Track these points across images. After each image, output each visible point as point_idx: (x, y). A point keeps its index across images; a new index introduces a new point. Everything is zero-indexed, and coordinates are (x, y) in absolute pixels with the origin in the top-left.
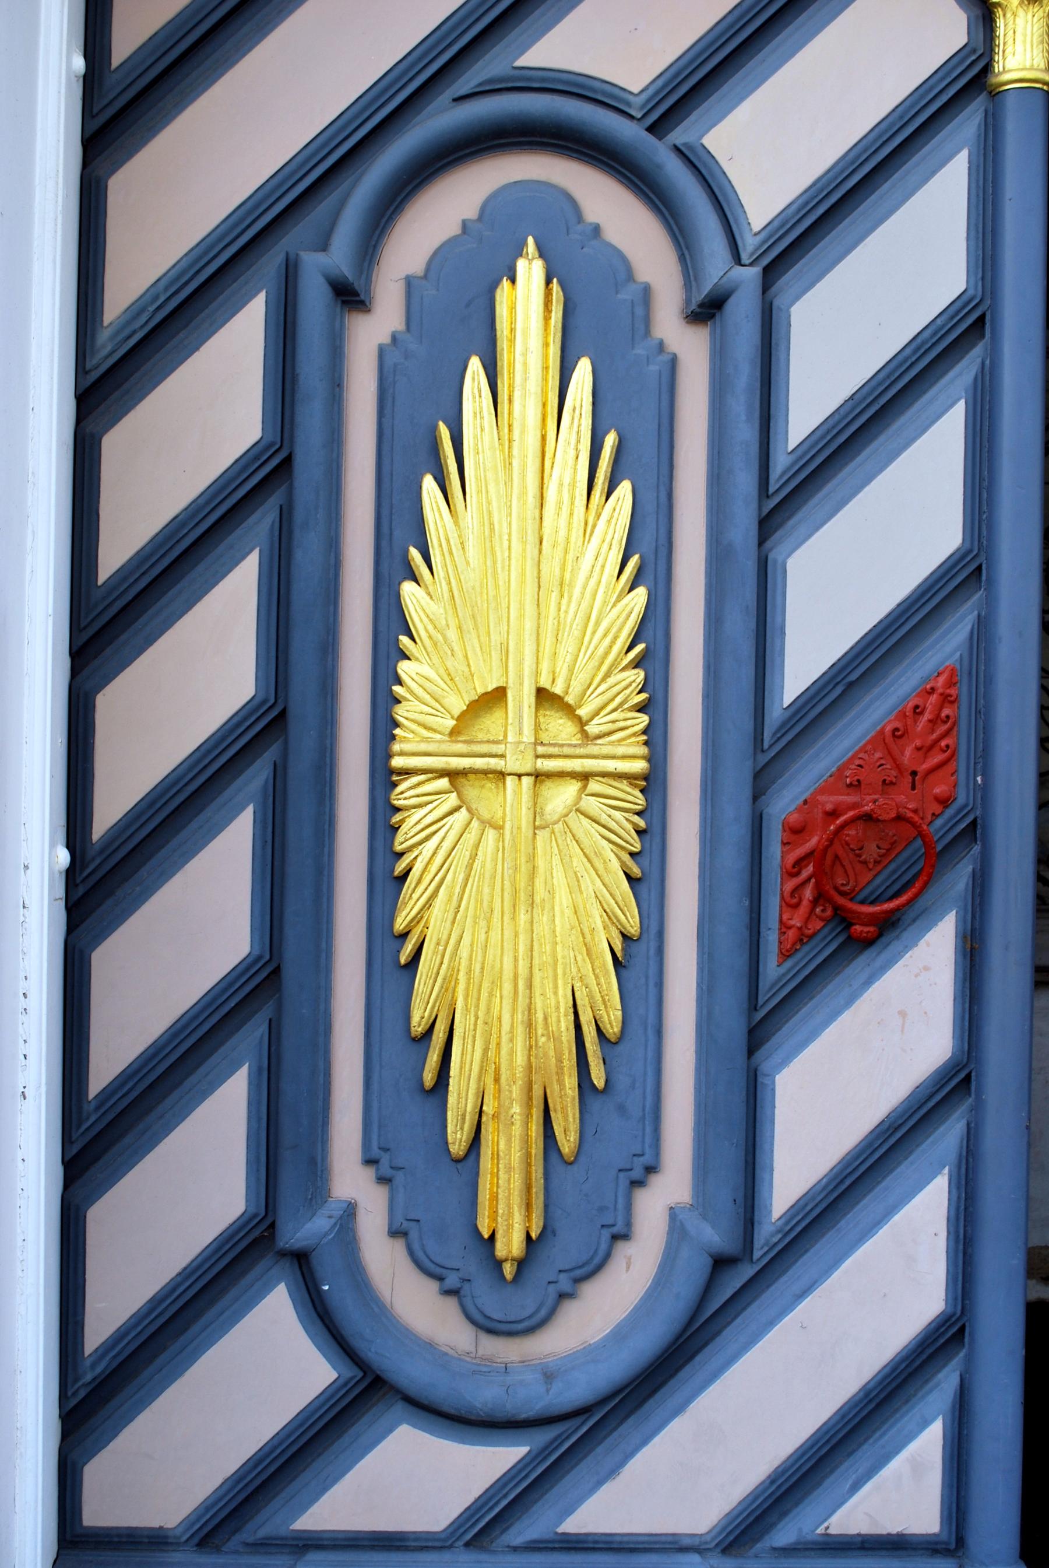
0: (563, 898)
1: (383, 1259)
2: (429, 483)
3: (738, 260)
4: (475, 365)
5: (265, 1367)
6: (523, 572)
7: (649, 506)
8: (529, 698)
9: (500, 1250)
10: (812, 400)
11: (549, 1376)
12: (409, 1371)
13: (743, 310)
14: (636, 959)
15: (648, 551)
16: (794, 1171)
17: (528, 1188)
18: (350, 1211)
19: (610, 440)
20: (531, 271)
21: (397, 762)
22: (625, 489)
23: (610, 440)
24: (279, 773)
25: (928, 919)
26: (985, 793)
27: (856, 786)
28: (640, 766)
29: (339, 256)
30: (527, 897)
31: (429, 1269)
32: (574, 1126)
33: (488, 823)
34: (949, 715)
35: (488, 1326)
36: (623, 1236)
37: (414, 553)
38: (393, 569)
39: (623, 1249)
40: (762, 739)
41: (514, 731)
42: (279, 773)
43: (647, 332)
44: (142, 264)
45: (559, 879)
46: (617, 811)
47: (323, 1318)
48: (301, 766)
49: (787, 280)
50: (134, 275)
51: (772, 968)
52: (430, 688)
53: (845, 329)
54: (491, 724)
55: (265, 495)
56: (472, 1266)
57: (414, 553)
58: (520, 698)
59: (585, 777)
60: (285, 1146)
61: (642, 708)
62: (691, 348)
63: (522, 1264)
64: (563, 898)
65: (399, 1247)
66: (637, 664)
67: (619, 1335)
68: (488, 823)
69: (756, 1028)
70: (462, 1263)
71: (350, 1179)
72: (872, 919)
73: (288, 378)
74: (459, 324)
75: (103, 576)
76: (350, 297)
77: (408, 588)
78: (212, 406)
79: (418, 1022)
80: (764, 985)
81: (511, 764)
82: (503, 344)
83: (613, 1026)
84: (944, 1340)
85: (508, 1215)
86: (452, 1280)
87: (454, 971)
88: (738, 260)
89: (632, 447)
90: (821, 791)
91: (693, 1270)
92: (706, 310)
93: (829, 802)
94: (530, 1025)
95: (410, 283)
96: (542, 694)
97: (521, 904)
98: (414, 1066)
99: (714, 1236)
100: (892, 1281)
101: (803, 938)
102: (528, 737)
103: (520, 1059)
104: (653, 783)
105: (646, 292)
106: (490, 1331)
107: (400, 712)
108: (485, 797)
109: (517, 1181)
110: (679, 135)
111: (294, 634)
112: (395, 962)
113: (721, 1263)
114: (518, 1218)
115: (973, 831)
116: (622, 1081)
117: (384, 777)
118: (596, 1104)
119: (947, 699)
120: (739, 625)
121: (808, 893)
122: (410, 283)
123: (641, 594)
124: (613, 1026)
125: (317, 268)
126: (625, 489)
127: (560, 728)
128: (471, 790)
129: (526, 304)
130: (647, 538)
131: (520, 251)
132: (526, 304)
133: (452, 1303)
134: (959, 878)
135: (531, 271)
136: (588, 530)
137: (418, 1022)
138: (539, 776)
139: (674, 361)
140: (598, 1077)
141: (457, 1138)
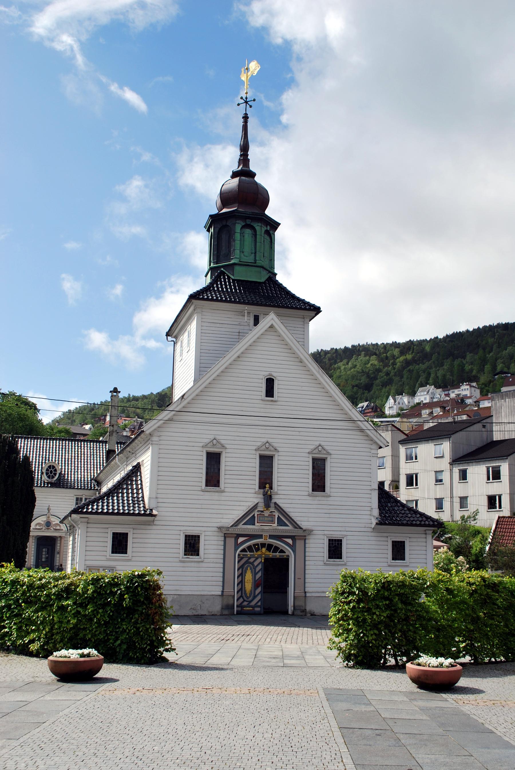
6: (249, 576)
53: (258, 569)
74: (247, 569)
85: (248, 595)
97: (248, 586)
98: (245, 591)
100: (259, 597)
112: (245, 588)
132: (249, 568)
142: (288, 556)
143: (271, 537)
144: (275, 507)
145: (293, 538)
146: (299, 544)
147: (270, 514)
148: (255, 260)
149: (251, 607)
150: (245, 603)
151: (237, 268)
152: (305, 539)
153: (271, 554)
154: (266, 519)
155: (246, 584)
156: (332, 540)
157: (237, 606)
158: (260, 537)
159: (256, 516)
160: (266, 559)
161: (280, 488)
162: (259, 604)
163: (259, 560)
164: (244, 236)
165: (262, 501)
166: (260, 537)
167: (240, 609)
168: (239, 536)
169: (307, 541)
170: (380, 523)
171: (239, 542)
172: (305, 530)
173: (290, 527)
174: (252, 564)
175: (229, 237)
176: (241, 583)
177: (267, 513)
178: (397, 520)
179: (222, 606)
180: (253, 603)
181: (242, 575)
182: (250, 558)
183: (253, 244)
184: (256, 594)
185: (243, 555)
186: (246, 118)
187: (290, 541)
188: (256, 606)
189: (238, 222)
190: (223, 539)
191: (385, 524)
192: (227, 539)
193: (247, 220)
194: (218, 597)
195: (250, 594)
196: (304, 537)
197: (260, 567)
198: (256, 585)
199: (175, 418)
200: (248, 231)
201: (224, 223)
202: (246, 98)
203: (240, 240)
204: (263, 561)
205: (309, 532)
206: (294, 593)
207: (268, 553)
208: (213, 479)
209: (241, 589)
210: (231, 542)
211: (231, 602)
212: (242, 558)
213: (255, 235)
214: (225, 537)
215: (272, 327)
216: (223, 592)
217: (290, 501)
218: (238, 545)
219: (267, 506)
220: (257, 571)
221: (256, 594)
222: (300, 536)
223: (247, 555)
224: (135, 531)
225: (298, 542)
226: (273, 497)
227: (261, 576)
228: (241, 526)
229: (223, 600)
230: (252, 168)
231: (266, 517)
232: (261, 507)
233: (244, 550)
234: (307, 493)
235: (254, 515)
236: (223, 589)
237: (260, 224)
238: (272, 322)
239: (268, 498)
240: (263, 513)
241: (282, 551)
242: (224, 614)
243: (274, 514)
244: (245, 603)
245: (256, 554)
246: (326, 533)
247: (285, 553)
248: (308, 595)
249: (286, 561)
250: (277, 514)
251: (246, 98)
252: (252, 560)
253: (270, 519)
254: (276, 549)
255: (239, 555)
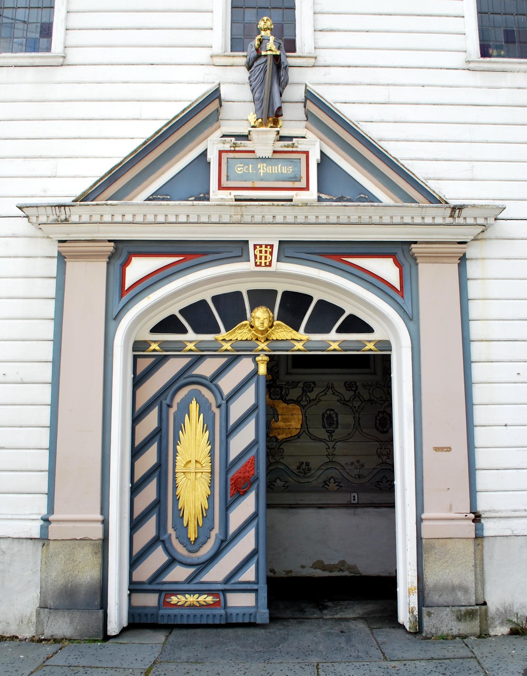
0: (199, 490)
1: (175, 542)
2: (180, 432)
3: (223, 399)
4: (187, 415)
5: (158, 558)
6: (193, 445)
7: (211, 434)
8: (194, 462)
9: (191, 540)
10: (233, 419)
11: (198, 558)
12: (178, 558)
13: (223, 407)
14: (210, 498)
15: (211, 441)
16: (233, 528)
17: (195, 531)
18: (170, 535)
19: (205, 425)
20: (194, 402)
21: (176, 471)
22: (208, 432)
23: (205, 425)
24: (160, 472)
25: (251, 491)
26: (258, 473)
27: (240, 473)
28: (210, 471)
29: (168, 401)
30: (194, 489)
31: (182, 543)
32: (201, 522)
33: (189, 479)
34: (253, 462)
35: (190, 552)
36: (209, 538)
37: (179, 442)
38: (175, 444)
39: (209, 540)
40: (227, 467)
41: (192, 465)
42: (160, 472)
43: (211, 410)
44: (141, 403)
45: (199, 487)
46: (206, 477)
47: (167, 550)
48: (163, 472)
49: (230, 402)
50: (140, 404)
51: (229, 499)
52: (181, 461)
53: (239, 408)
54: (189, 465)
55: (159, 434)
56: (187, 543)
57: (179, 442)
58: (193, 462)
59: (202, 472)
60: (161, 526)
61: (210, 463)
62: (217, 411)
63: (194, 541)
64: (199, 490)
65: (177, 540)
66: (210, 456)
67: (208, 552)
68: (189, 479)
69: (227, 507)
70: (185, 541)
71: (170, 530)
72: (242, 492)
73: (162, 418)
74: (184, 409)
75: (136, 446)
76: (169, 406)
77: (178, 446)
78: (151, 422)
79: (177, 494)
80: (228, 501)
81: (192, 471)
82: (191, 413)
83: (207, 508)
84: (254, 553)
85: (192, 536)
86: (185, 545)
87: (184, 500)
88: (223, 399)
89: (209, 426)
90: (236, 473)
91: (219, 542)
92: (219, 406)
93: (236, 475)
94: (195, 507)
95: (178, 403)
96: (196, 461)
97: (193, 491)
98: (179, 514)
99: (222, 537)
100: (247, 544)
101: (233, 495)
102: (194, 467)
103: (194, 512)
104: (212, 473)
105: (211, 404)
106: (190, 552)
107: (177, 464)
108: (188, 475)
109: (193, 530)
110: (215, 382)
111: (162, 454)
112: (176, 499)
113: (222, 541)
114: (194, 535)
115: (257, 479)
116: (208, 516)
117: (175, 473)
118: (205, 519)
119: (252, 460)
120: (224, 451)
121: (234, 488)
122: (178, 403)
123: (210, 446)
124: (207, 508)
125: (165, 403)
126: (208, 432)
127: (198, 465)
128: (187, 474)
129: (194, 407)
130: (211, 439)
131: (193, 400)
132: (194, 407)
133: (185, 548)
134: (255, 486)
135: (194, 402)
136: (202, 438)
137: (177, 494)
138: (196, 472)
139: (214, 414)
140: (205, 515)
141: (185, 524)
142: (386, 345)
143: (290, 250)
144: (309, 115)
145: (400, 251)
146: (435, 281)
147: (280, 146)
149: (209, 592)
150: (179, 574)
152: (463, 259)
153: (299, 340)
154: (263, 169)
155: (180, 478)
158: (238, 249)
159: (213, 157)
160: (274, 362)
161: (325, 39)
162: (249, 574)
163: (243, 368)
166: (238, 249)
168: (123, 251)
169: (472, 269)
171: (129, 282)
172: (456, 209)
176: (154, 478)
179: (42, 593)
180: (217, 573)
182: (198, 360)
185: (162, 344)
187: (386, 269)
188: (231, 584)
192: (71, 266)
196: (460, 249)
197: (248, 399)
198: (235, 488)
204: (263, 370)
205: (486, 221)
206: (419, 521)
207: (283, 332)
210: (90, 278)
211: (89, 574)
212: (160, 361)
214: (62, 258)
217: (380, 94)
218: (123, 292)
220: (234, 417)
221: (233, 528)
223: (180, 346)
225: (425, 271)
227: (255, 443)
229: (46, 563)
231: (263, 159)
232: (240, 111)
234: (458, 60)
235: (204, 154)
236: (51, 509)
240: (247, 145)
241: (355, 325)
242: (48, 633)
245: (226, 338)
247: (368, 329)
248: (490, 528)
249: (378, 367)
250: (314, 145)
252: (207, 368)
253: (286, 170)
254: (327, 315)
255: (139, 347)
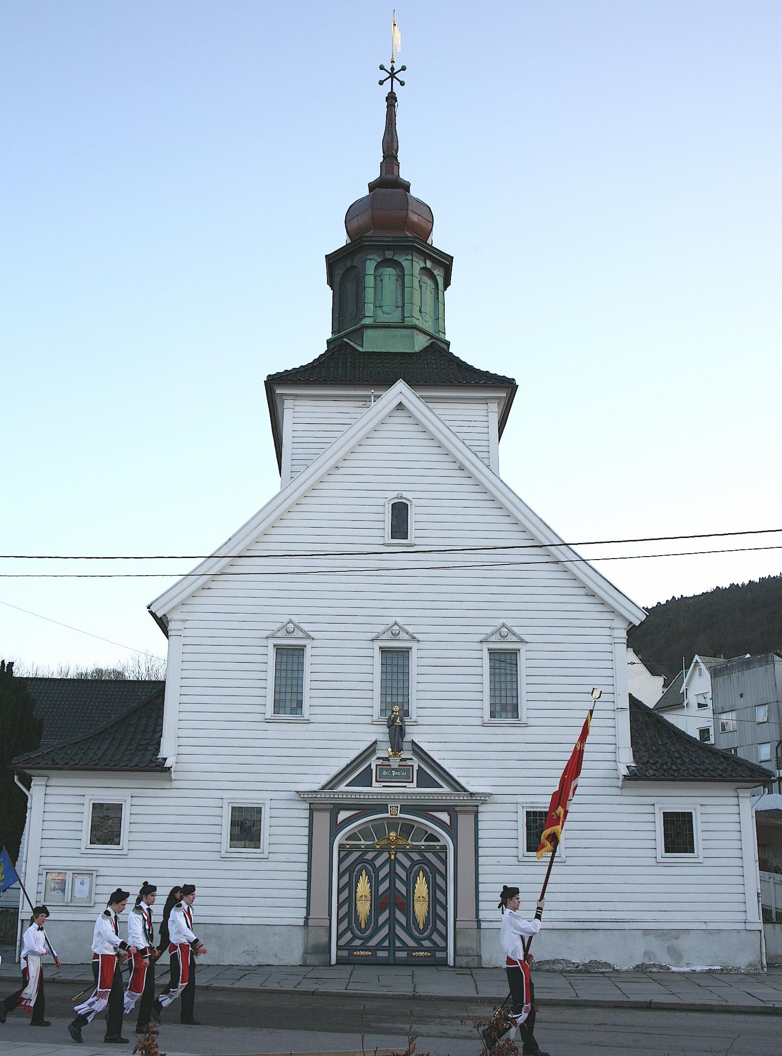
98: (357, 917)
143: (405, 809)
144: (414, 750)
145: (451, 810)
146: (465, 822)
148: (403, 317)
150: (357, 942)
151: (368, 334)
155: (359, 903)
156: (535, 812)
157: (339, 948)
158: (383, 808)
159: (373, 767)
164: (382, 280)
165: (386, 738)
167: (345, 953)
168: (337, 808)
170: (633, 777)
172: (471, 794)
173: (446, 789)
174: (371, 862)
175: (357, 285)
176: (349, 901)
177: (395, 763)
178: (671, 768)
180: (373, 942)
181: (350, 887)
183: (399, 291)
184: (380, 924)
186: (391, 99)
187: (445, 817)
189: (369, 257)
190: (306, 814)
191: (645, 778)
193: (387, 253)
194: (298, 930)
195: (368, 924)
199: (213, 585)
200: (389, 272)
201: (349, 264)
202: (392, 69)
203: (375, 287)
205: (485, 798)
208: (288, 699)
209: (348, 914)
210: (323, 820)
212: (349, 853)
213: (401, 277)
214: (311, 811)
215: (400, 406)
216: (307, 919)
219: (397, 748)
221: (380, 924)
222: (465, 807)
224: (135, 801)
226: (408, 729)
228: (342, 788)
229: (307, 935)
230: (405, 174)
232: (384, 751)
233: (352, 837)
236: (308, 913)
237: (410, 257)
238: (400, 398)
239: (397, 732)
242: (308, 962)
243: (409, 763)
244: (357, 942)
246: (521, 799)
250: (416, 763)
251: (392, 69)
255: (341, 846)
